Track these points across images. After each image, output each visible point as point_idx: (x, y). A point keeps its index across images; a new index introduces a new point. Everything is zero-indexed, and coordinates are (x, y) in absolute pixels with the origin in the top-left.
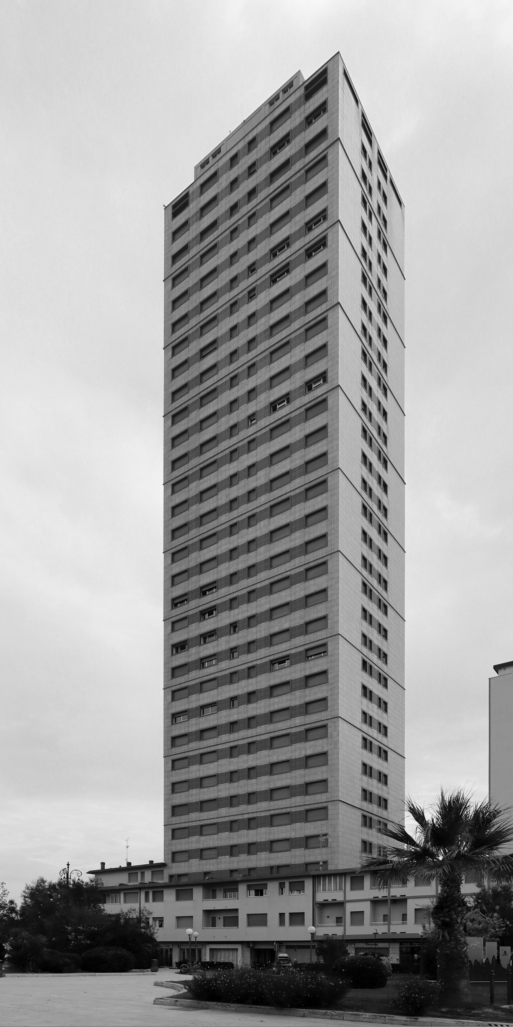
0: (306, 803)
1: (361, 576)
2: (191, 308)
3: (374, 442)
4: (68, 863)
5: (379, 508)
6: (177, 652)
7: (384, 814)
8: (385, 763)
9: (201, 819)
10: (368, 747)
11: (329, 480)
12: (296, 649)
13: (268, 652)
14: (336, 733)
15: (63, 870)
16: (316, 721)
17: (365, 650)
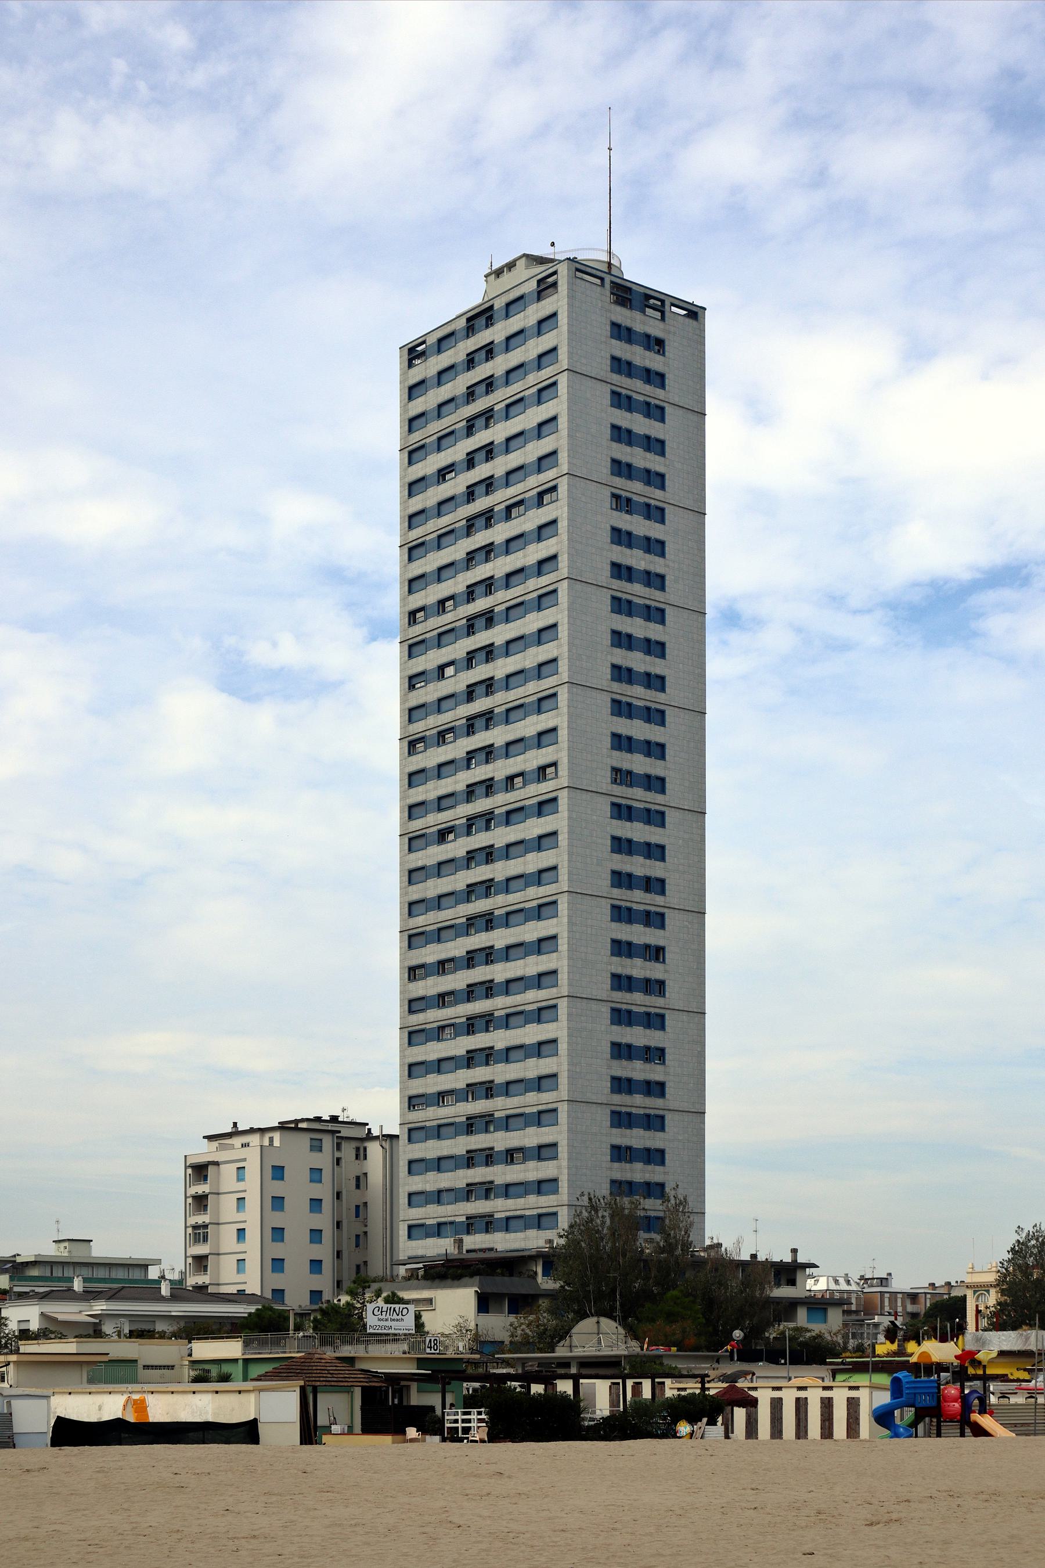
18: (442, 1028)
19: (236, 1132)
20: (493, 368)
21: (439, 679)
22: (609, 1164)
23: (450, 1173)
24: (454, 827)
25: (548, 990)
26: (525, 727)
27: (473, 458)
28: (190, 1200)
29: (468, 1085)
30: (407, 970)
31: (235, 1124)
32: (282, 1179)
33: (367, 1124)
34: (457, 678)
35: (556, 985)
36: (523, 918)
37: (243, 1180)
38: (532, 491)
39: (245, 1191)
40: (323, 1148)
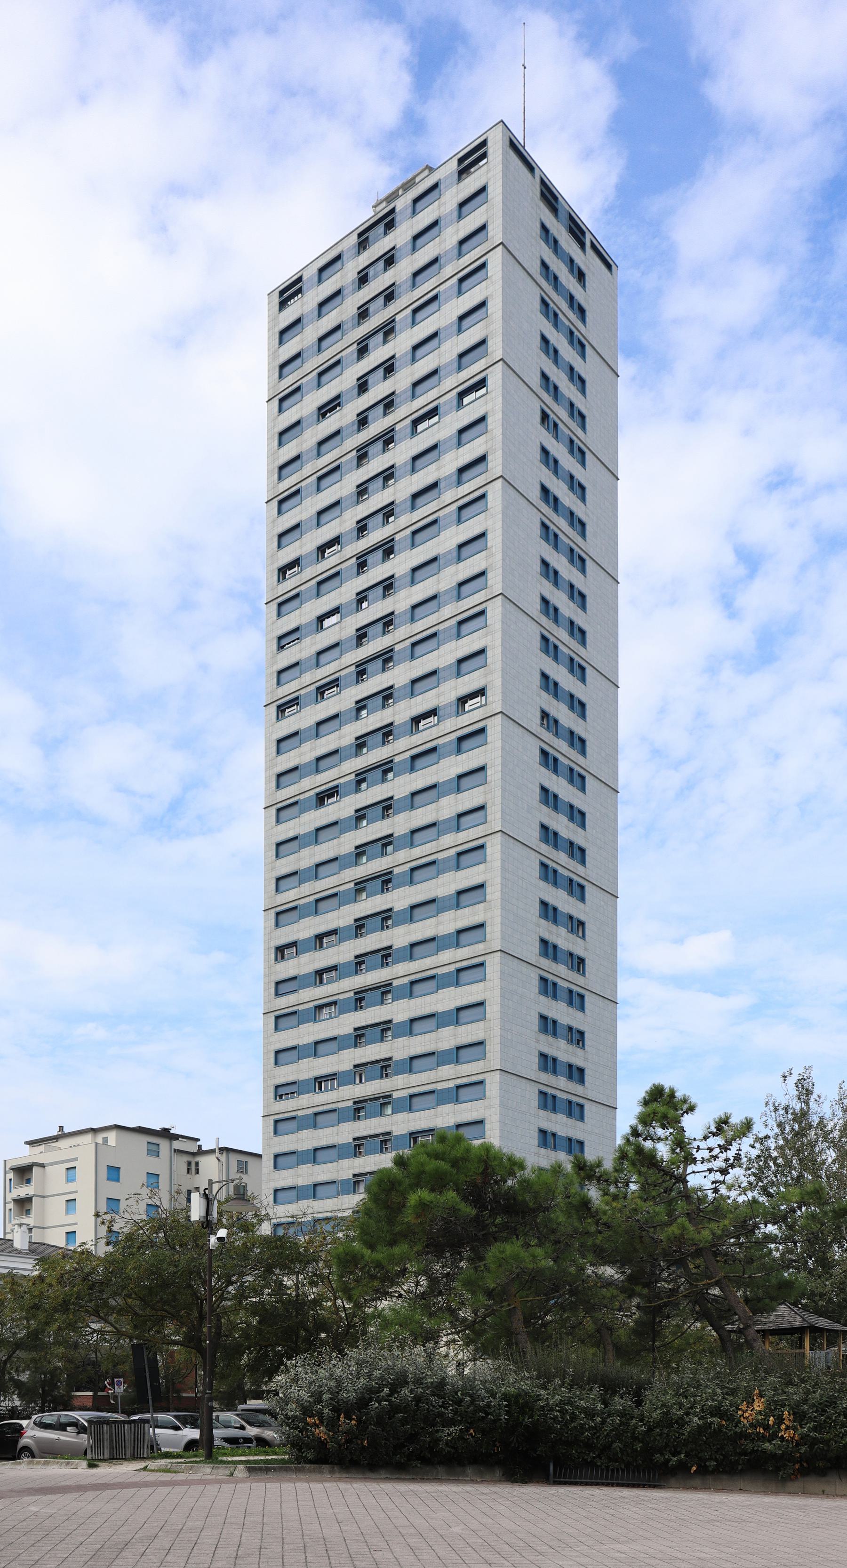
1: (539, 627)
3: (562, 431)
5: (572, 415)
7: (580, 980)
8: (580, 905)
10: (549, 991)
11: (488, 610)
17: (547, 736)
18: (320, 1008)
19: (62, 1135)
20: (395, 276)
21: (317, 631)
22: (537, 1149)
23: (330, 1165)
24: (337, 786)
25: (470, 947)
26: (439, 657)
27: (366, 382)
28: (11, 1206)
29: (355, 1066)
30: (273, 951)
31: (61, 1128)
32: (118, 1180)
33: (199, 1140)
34: (343, 624)
35: (484, 940)
36: (436, 872)
37: (73, 1180)
38: (450, 393)
39: (76, 1192)
40: (160, 1153)
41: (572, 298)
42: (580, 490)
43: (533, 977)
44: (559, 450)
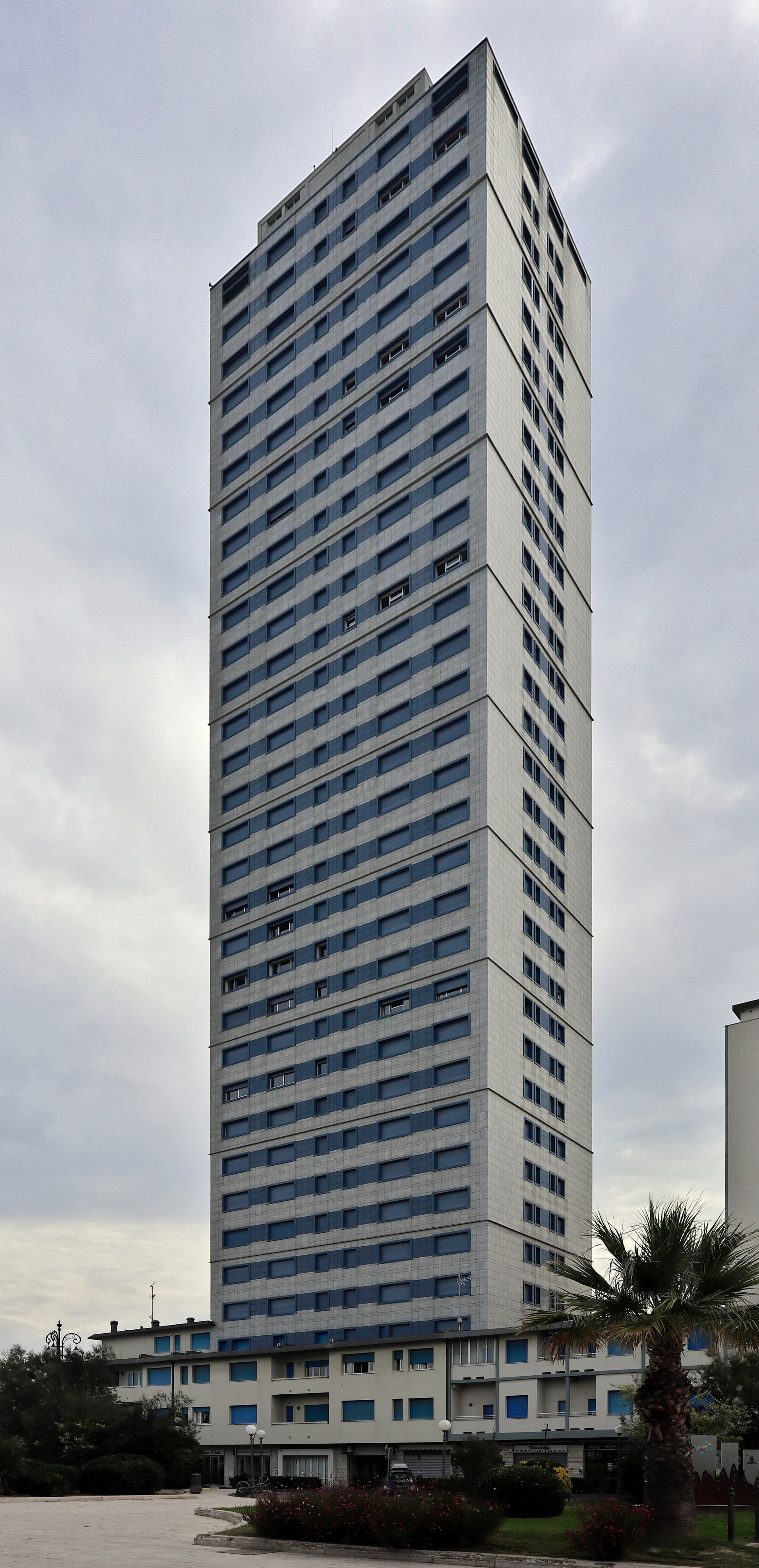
0: (435, 1226)
2: (252, 446)
4: (59, 1322)
5: (551, 758)
6: (231, 989)
7: (559, 1125)
9: (269, 1252)
12: (420, 982)
13: (376, 987)
14: (482, 1115)
15: (52, 1334)
16: (451, 1095)
17: (529, 984)
35: (468, 1206)
41: (551, 632)
42: (558, 838)
43: (520, 1241)
44: (541, 798)
